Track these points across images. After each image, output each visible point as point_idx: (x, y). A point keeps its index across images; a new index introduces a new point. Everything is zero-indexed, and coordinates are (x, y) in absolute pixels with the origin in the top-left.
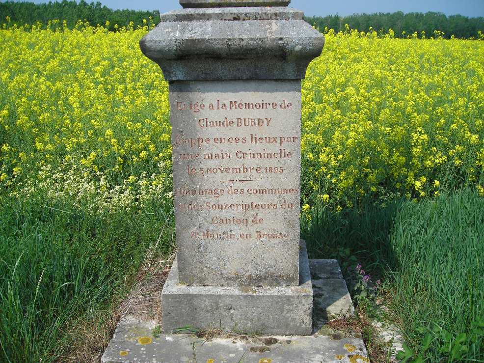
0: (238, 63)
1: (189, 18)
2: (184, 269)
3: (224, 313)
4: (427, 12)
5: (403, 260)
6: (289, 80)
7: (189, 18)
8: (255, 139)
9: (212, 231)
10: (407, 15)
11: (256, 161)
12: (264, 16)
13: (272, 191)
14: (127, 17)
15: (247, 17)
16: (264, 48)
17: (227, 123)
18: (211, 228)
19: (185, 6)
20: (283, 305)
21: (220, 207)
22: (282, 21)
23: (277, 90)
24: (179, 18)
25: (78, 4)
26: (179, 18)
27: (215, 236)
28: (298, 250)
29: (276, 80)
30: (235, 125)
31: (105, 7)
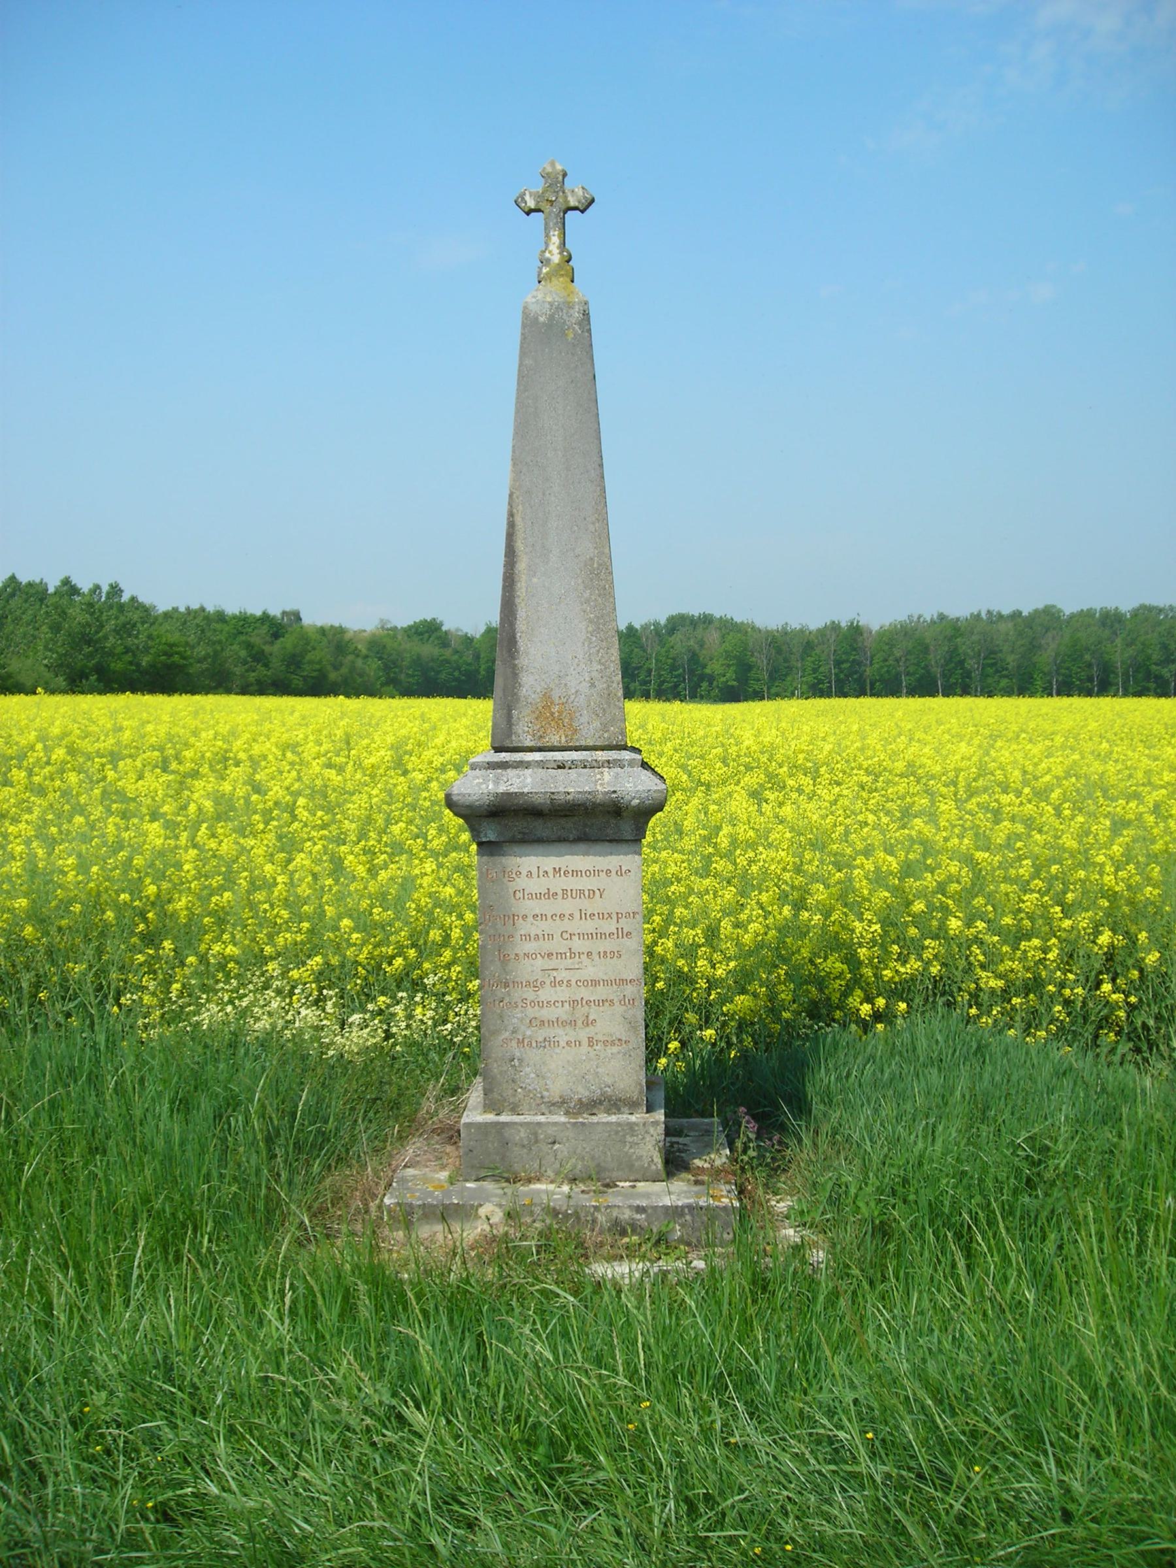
0: (563, 821)
1: (504, 765)
2: (491, 1091)
3: (546, 1148)
4: (1136, 605)
5: (817, 1108)
6: (627, 841)
7: (504, 765)
8: (583, 915)
9: (530, 1036)
10: (1072, 616)
11: (587, 943)
12: (595, 764)
13: (607, 983)
14: (203, 631)
15: (574, 765)
16: (594, 803)
17: (550, 895)
18: (528, 1033)
19: (497, 750)
20: (624, 1136)
21: (541, 1004)
22: (615, 770)
23: (611, 854)
24: (492, 766)
25: (51, 590)
26: (492, 766)
27: (534, 1044)
28: (643, 1063)
29: (610, 841)
30: (560, 896)
31: (133, 599)
